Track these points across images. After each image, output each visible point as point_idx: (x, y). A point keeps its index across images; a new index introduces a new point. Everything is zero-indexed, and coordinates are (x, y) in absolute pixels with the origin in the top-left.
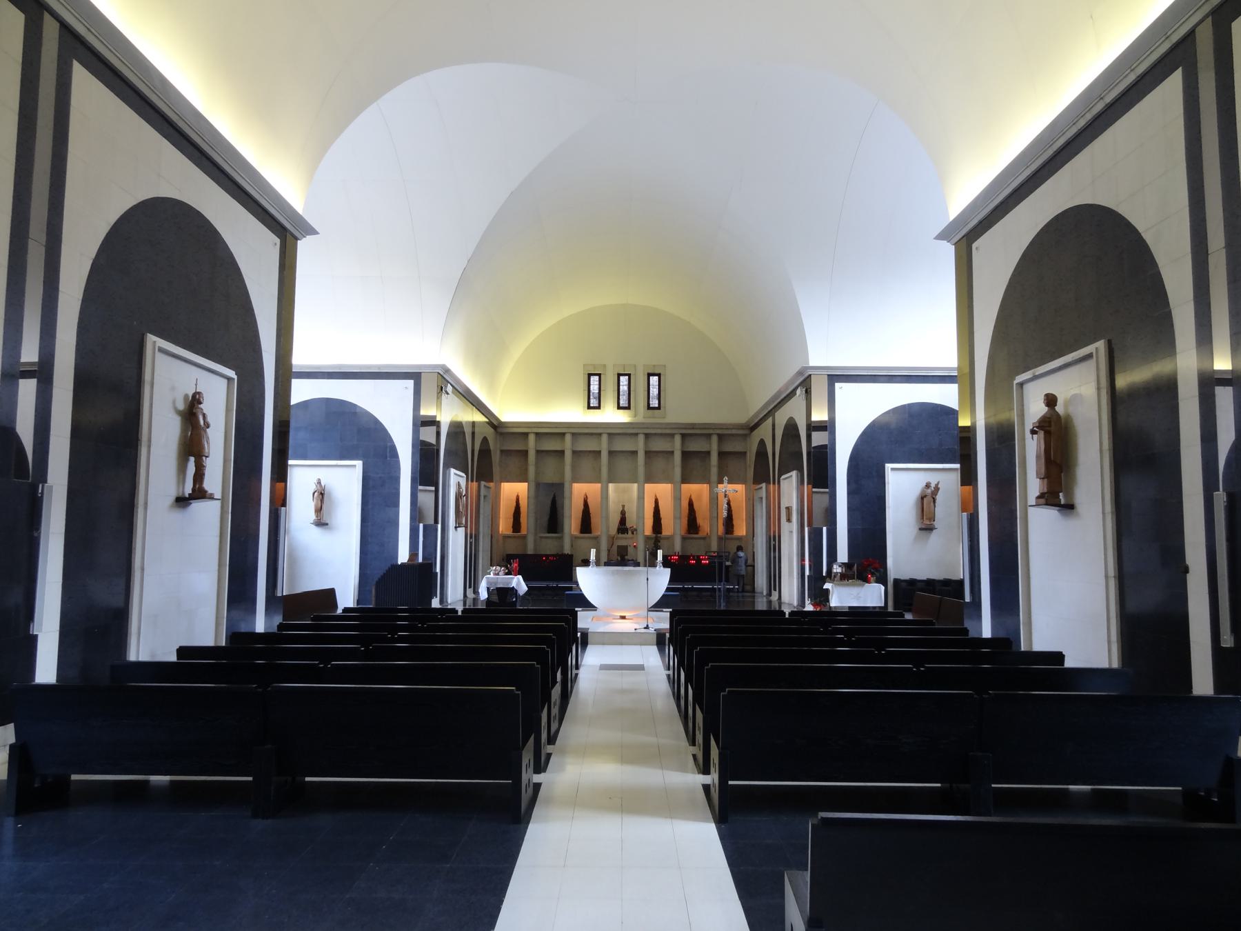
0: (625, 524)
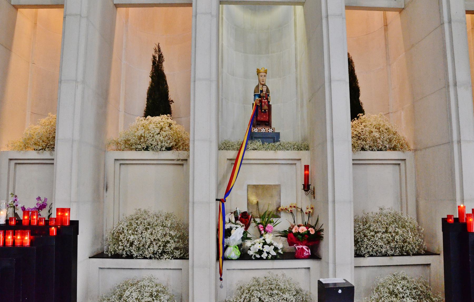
0: (268, 123)
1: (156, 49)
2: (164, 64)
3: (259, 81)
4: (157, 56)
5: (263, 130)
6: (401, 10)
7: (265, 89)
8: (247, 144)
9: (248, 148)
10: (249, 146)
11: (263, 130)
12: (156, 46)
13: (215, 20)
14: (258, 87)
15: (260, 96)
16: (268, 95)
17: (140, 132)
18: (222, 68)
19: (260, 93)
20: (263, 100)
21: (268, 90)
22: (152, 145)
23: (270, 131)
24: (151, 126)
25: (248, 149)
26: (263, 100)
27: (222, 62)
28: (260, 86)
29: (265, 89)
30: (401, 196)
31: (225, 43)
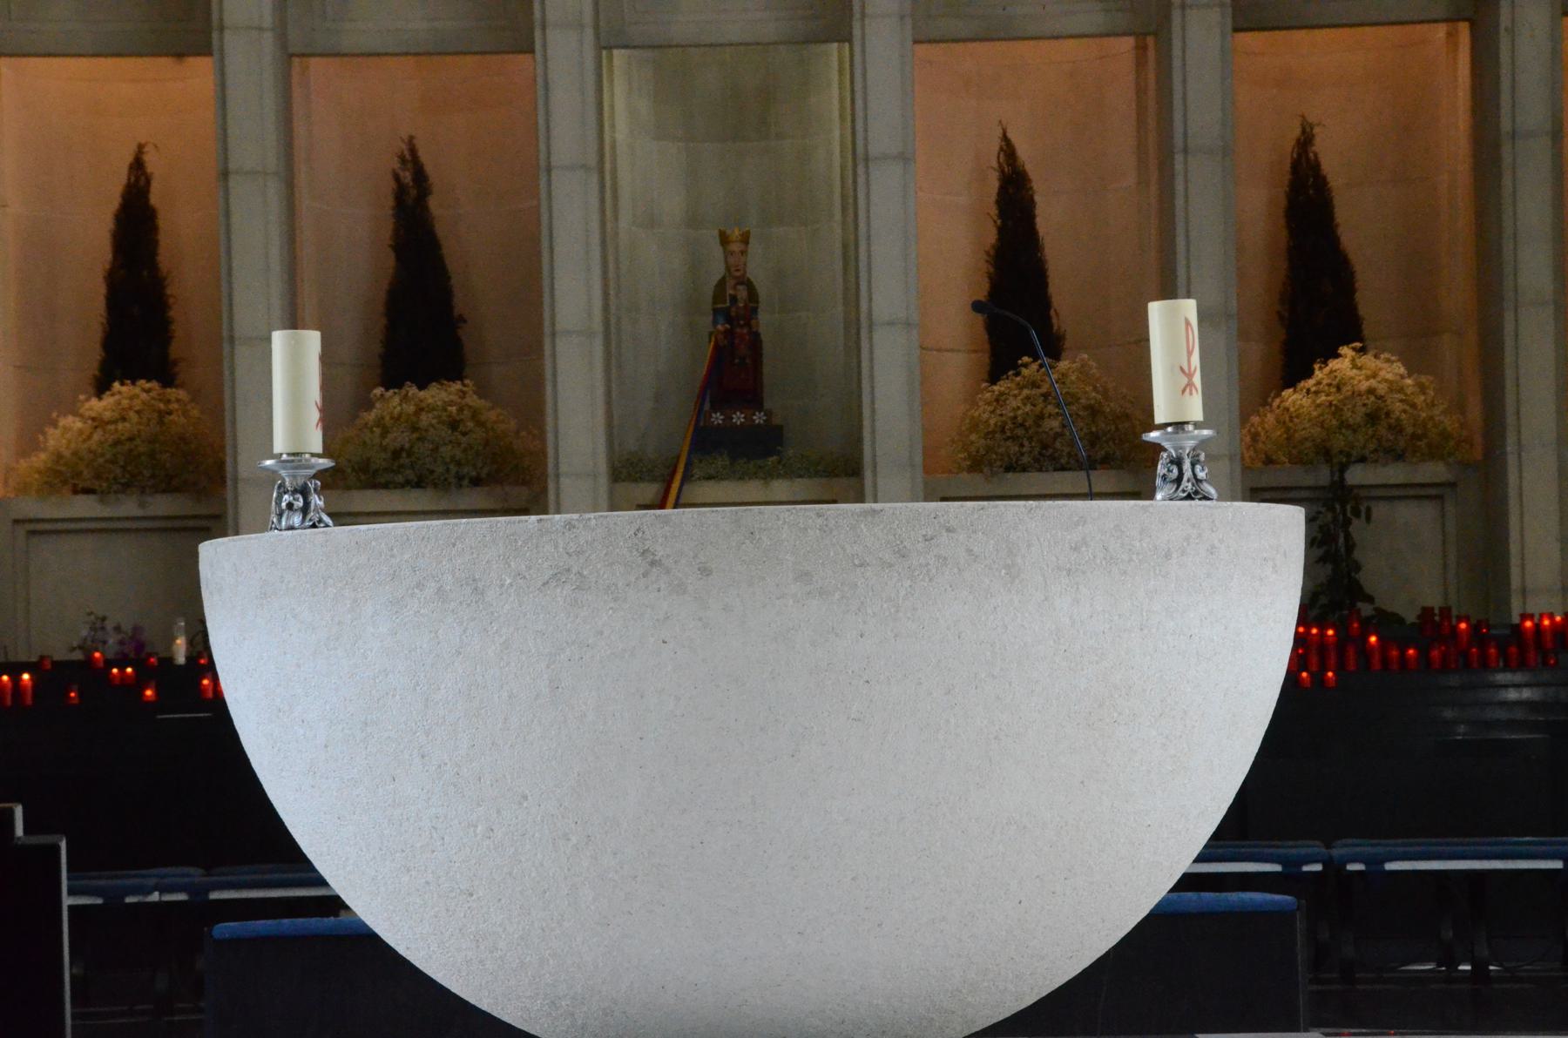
0: (752, 396)
1: (402, 152)
2: (433, 203)
3: (728, 268)
4: (407, 177)
5: (738, 418)
6: (1155, 34)
7: (742, 293)
8: (688, 465)
9: (692, 476)
10: (697, 472)
11: (738, 418)
12: (404, 147)
13: (594, 179)
14: (722, 283)
15: (729, 319)
16: (755, 310)
17: (400, 437)
18: (616, 219)
19: (728, 304)
20: (738, 330)
21: (753, 295)
22: (432, 472)
23: (759, 418)
24: (425, 419)
25: (693, 479)
26: (738, 330)
27: (615, 197)
28: (730, 283)
29: (742, 293)
30: (137, 530)
31: (621, 135)
